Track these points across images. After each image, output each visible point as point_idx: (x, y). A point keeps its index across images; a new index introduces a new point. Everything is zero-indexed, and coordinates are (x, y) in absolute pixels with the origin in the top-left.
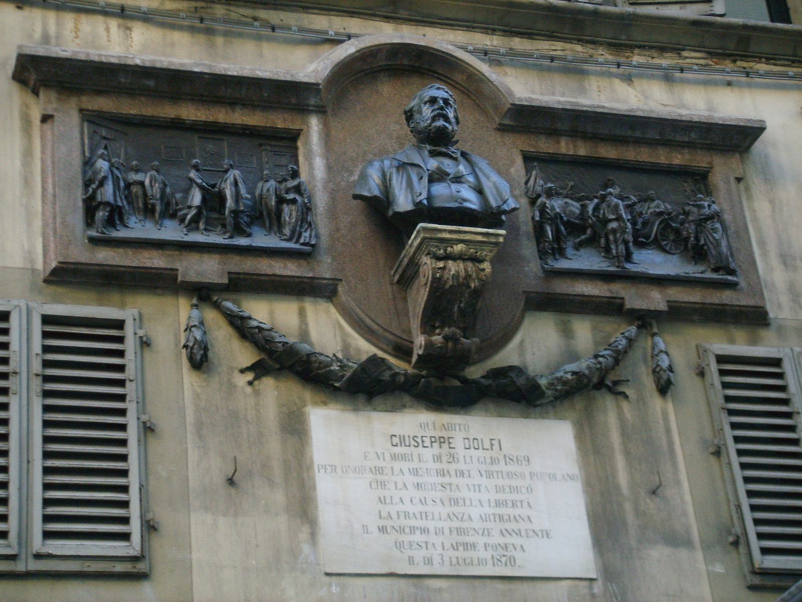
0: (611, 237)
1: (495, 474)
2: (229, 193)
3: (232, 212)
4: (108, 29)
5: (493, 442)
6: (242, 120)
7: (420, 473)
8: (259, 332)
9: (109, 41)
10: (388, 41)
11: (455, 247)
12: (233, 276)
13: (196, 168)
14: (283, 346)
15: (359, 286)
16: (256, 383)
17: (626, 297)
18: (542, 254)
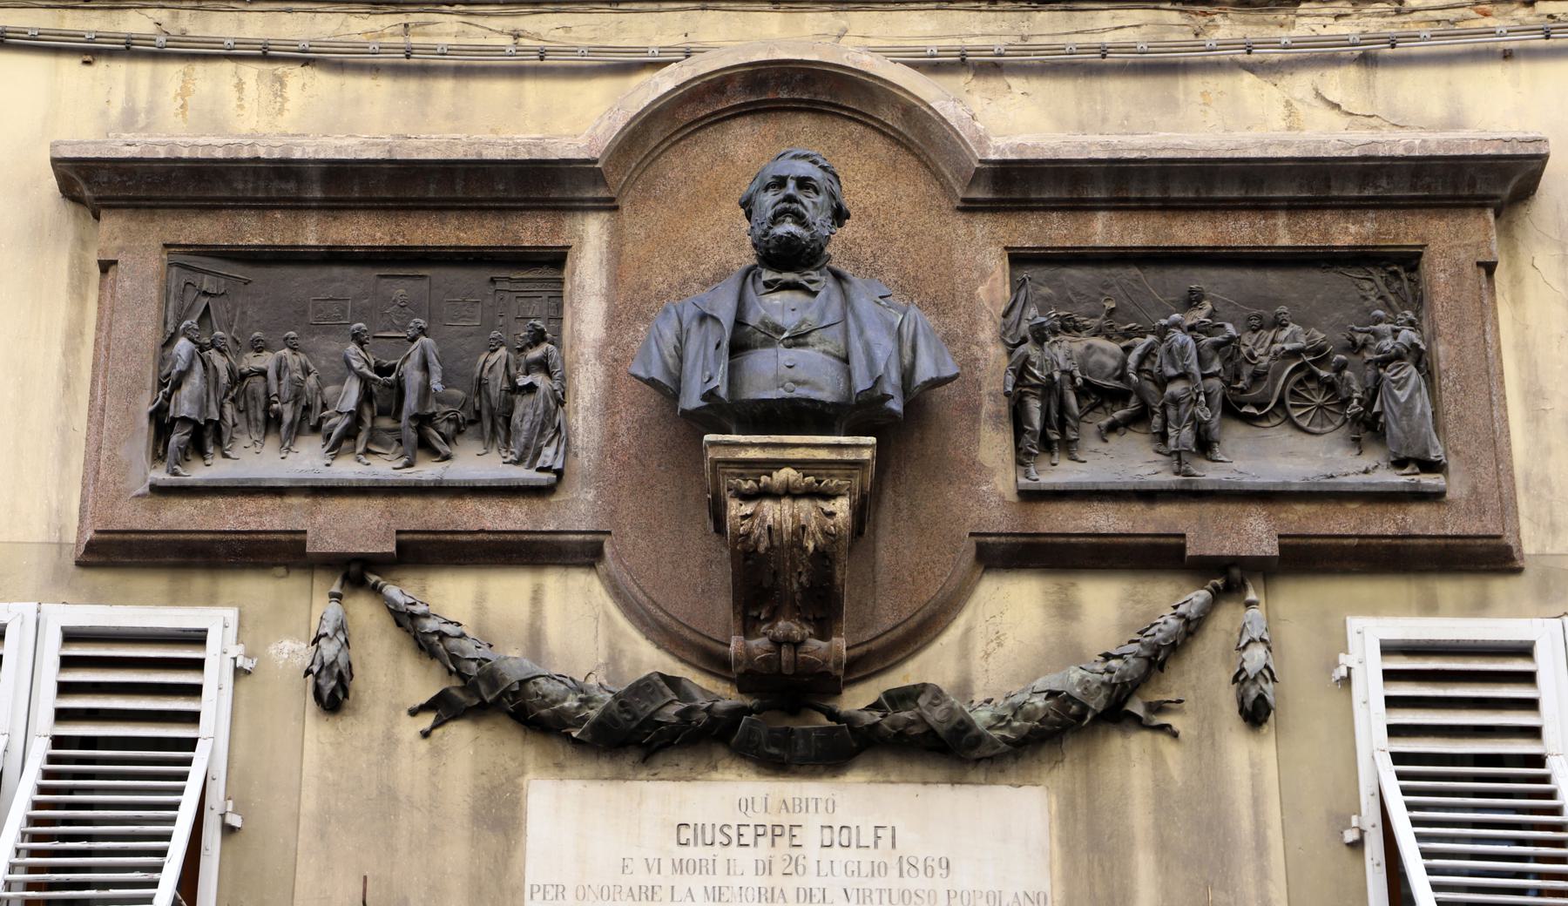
0: (1171, 412)
1: (875, 896)
2: (413, 378)
3: (414, 417)
4: (240, 86)
5: (880, 832)
6: (458, 238)
7: (727, 895)
8: (441, 640)
9: (241, 107)
10: (743, 60)
11: (775, 474)
12: (404, 537)
13: (358, 338)
14: (479, 665)
15: (642, 544)
16: (438, 732)
17: (1190, 534)
18: (1022, 458)
